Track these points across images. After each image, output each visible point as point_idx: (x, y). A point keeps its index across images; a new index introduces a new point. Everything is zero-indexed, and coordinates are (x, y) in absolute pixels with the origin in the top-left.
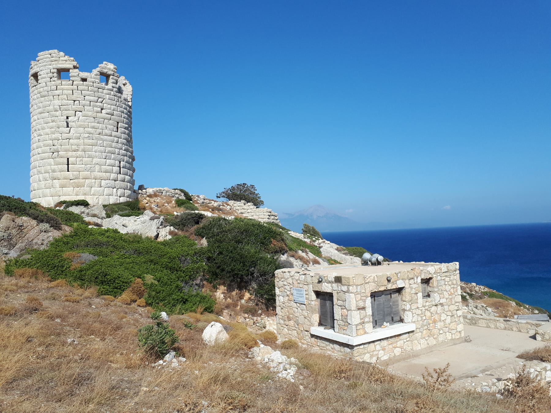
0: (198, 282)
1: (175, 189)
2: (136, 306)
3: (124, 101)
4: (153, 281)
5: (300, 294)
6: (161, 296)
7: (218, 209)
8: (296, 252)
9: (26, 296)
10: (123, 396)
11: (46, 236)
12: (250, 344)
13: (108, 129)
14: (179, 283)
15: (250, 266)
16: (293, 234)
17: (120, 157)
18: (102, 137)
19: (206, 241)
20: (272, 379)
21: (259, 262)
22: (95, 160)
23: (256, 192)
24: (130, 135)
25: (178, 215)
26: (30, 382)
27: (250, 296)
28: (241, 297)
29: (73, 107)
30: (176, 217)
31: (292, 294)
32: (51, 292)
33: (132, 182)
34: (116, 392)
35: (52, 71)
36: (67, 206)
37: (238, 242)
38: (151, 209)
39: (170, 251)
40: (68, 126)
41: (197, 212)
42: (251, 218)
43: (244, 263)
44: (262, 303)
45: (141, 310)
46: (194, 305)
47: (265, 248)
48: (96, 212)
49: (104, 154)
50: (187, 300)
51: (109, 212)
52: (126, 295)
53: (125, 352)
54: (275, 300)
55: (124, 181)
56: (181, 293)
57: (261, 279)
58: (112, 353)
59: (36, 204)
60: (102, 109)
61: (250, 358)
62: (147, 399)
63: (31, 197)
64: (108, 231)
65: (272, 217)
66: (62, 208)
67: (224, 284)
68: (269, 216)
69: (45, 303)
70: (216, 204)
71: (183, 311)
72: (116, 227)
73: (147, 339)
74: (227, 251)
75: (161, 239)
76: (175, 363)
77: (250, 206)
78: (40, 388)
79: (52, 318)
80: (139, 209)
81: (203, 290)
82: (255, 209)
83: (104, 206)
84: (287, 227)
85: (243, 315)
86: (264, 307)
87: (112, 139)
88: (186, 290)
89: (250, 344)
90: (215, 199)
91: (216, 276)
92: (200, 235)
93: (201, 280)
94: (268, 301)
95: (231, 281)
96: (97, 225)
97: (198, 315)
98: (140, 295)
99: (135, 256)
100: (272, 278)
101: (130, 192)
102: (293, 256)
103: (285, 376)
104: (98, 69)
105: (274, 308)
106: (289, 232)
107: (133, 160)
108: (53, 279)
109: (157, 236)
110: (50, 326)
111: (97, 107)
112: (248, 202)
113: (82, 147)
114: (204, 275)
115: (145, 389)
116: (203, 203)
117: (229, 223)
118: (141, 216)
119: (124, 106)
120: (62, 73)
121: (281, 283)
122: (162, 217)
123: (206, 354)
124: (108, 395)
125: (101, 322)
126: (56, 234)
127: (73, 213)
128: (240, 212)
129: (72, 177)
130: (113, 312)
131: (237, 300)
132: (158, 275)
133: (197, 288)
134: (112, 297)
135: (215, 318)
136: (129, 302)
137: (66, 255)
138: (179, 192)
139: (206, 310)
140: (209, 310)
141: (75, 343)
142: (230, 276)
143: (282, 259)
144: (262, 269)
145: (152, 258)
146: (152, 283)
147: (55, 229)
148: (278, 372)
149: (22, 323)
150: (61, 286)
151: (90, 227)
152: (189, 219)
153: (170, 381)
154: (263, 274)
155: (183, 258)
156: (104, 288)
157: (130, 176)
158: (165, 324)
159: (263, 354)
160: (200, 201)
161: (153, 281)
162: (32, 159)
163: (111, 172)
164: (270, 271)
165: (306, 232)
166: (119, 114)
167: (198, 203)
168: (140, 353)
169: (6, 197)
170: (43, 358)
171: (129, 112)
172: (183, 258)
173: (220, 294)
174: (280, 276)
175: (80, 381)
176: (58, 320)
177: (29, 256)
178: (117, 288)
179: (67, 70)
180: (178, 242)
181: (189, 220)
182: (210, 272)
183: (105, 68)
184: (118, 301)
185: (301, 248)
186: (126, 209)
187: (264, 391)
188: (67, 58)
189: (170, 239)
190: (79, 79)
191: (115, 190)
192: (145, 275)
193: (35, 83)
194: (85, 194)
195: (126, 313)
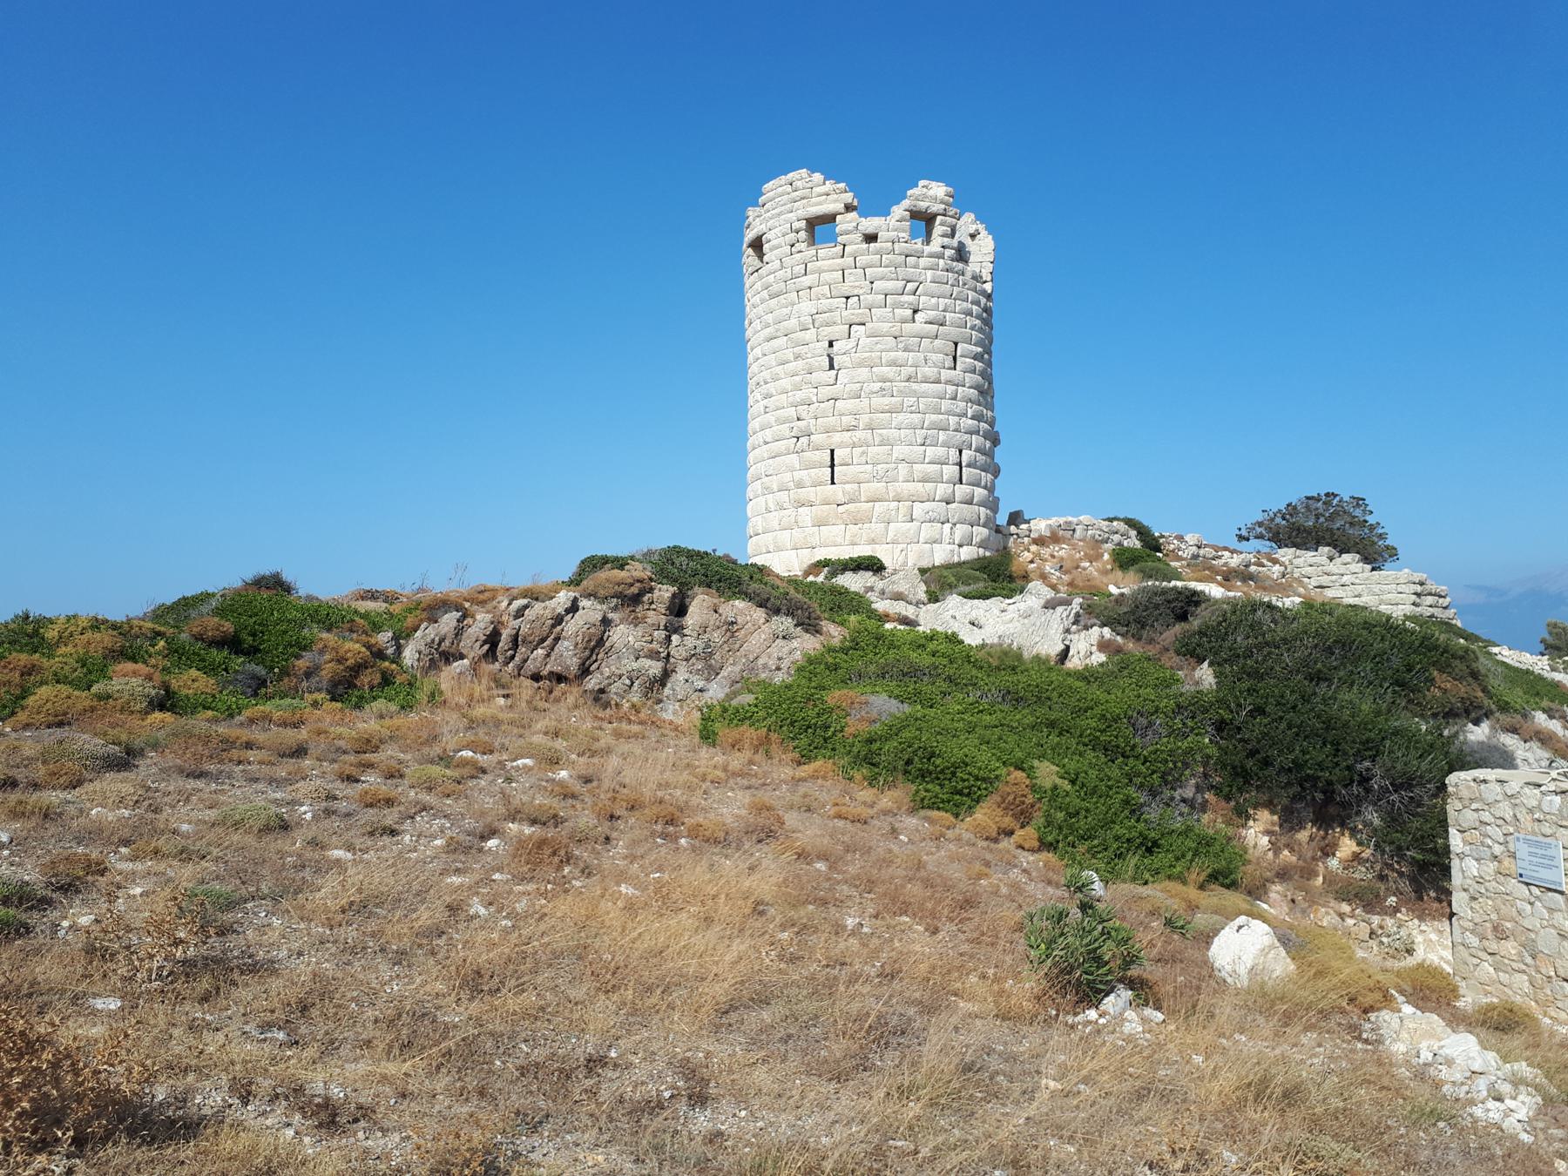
0: (1189, 793)
1: (1111, 520)
2: (1012, 848)
3: (972, 283)
4: (1059, 781)
5: (1544, 857)
6: (1082, 824)
7: (1244, 575)
8: (1525, 716)
9: (744, 798)
10: (994, 1095)
11: (786, 650)
12: (1363, 1002)
13: (930, 363)
14: (1131, 791)
15: (1360, 757)
16: (1506, 654)
17: (961, 437)
18: (915, 386)
19: (1210, 671)
20: (1451, 1119)
21: (1387, 743)
22: (900, 451)
23: (1371, 520)
24: (986, 376)
25: (1122, 595)
26: (766, 1015)
27: (1356, 849)
28: (1328, 851)
29: (845, 313)
30: (1117, 601)
31: (1513, 856)
32: (802, 789)
33: (992, 504)
34: (975, 1080)
35: (797, 225)
36: (833, 574)
37: (1317, 678)
38: (1044, 577)
39: (1103, 697)
40: (832, 367)
41: (1179, 584)
42: (1352, 601)
43: (1336, 744)
44: (1401, 874)
45: (1026, 859)
46: (1178, 859)
47: (1410, 701)
48: (902, 587)
49: (921, 433)
50: (1155, 844)
51: (933, 588)
52: (985, 815)
53: (991, 972)
54: (1446, 871)
55: (970, 502)
56: (1138, 821)
57: (1394, 797)
58: (958, 968)
59: (762, 570)
60: (915, 312)
61: (1366, 1041)
62: (1058, 1113)
63: (750, 551)
64: (932, 637)
65: (1430, 600)
66: (820, 579)
67: (1270, 805)
68: (1418, 595)
69: (791, 819)
70: (1235, 561)
71: (1147, 876)
72: (954, 627)
73: (1051, 943)
74: (1279, 704)
75: (1074, 663)
76: (1133, 1023)
77: (1350, 563)
78: (790, 1036)
79: (802, 855)
80: (1011, 578)
81: (1206, 818)
82: (1367, 574)
83: (923, 571)
84: (1482, 633)
85: (1333, 903)
86: (1405, 886)
87: (943, 393)
88: (1153, 813)
89: (1368, 1000)
90: (1234, 543)
91: (1245, 776)
92: (1193, 652)
93: (1198, 788)
94: (1424, 873)
95: (1294, 799)
96: (905, 621)
97: (1192, 892)
98: (1024, 818)
99: (1005, 707)
100: (1435, 796)
101: (985, 531)
102: (1514, 730)
103: (1495, 1116)
104: (906, 203)
105: (1445, 895)
106: (1495, 650)
107: (996, 441)
108: (804, 758)
109: (1064, 654)
110: (805, 879)
111: (902, 307)
112: (1341, 552)
113: (865, 419)
114: (1205, 775)
115: (1052, 1084)
116: (1195, 557)
117: (1284, 618)
118: (1017, 598)
119: (971, 295)
120: (818, 227)
121: (1469, 817)
122: (1078, 601)
123: (1226, 1010)
124: (955, 1084)
125: (928, 883)
126: (807, 644)
127: (847, 591)
128: (1314, 582)
129: (841, 498)
130: (952, 859)
131: (1314, 858)
132: (1072, 766)
133: (1186, 810)
134: (947, 817)
135: (1245, 906)
136: (994, 834)
137: (834, 697)
138: (1122, 526)
139: (1214, 877)
140: (1223, 878)
141: (865, 930)
142: (1289, 784)
143: (1471, 737)
144: (1399, 766)
145: (1054, 716)
146: (1055, 787)
147: (807, 631)
148: (1472, 1103)
149: (744, 866)
150: (824, 778)
151: (888, 626)
152: (1157, 607)
153: (1121, 1074)
154: (1405, 783)
155: (1143, 721)
156: (927, 791)
157: (985, 487)
158: (1100, 906)
159: (1409, 1033)
160: (1187, 553)
161: (1059, 781)
162: (751, 457)
163: (939, 479)
164: (1428, 776)
165: (1558, 649)
166: (960, 321)
167: (1180, 559)
168: (1031, 983)
169: (698, 553)
170: (793, 959)
171: (986, 310)
172: (1143, 721)
173: (1257, 834)
174: (1465, 793)
175: (886, 1034)
176: (821, 866)
177: (750, 698)
178: (960, 793)
179: (830, 219)
180: (1125, 673)
181: (1158, 611)
182: (1224, 766)
183: (924, 197)
184: (964, 829)
185: (1545, 703)
186: (977, 580)
187: (1424, 1155)
188: (829, 185)
189: (1102, 665)
190: (858, 237)
191: (947, 526)
192: (1036, 763)
193: (757, 262)
194: (873, 542)
195: (987, 864)
